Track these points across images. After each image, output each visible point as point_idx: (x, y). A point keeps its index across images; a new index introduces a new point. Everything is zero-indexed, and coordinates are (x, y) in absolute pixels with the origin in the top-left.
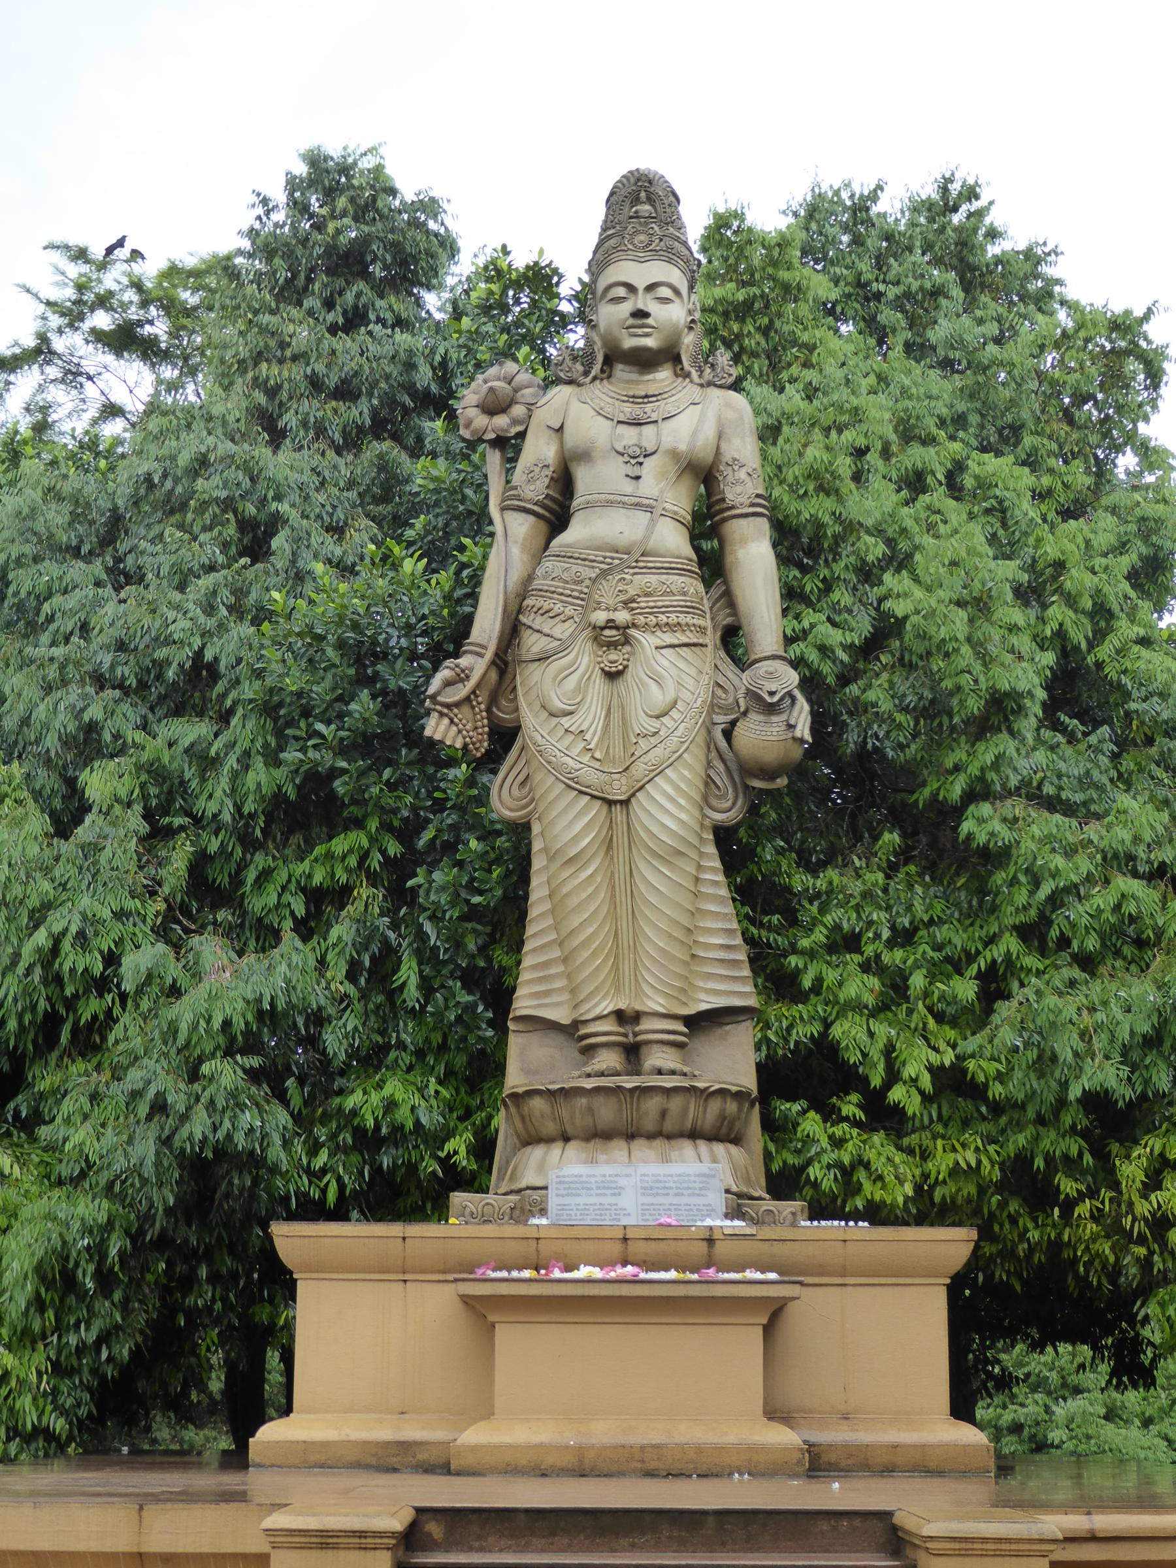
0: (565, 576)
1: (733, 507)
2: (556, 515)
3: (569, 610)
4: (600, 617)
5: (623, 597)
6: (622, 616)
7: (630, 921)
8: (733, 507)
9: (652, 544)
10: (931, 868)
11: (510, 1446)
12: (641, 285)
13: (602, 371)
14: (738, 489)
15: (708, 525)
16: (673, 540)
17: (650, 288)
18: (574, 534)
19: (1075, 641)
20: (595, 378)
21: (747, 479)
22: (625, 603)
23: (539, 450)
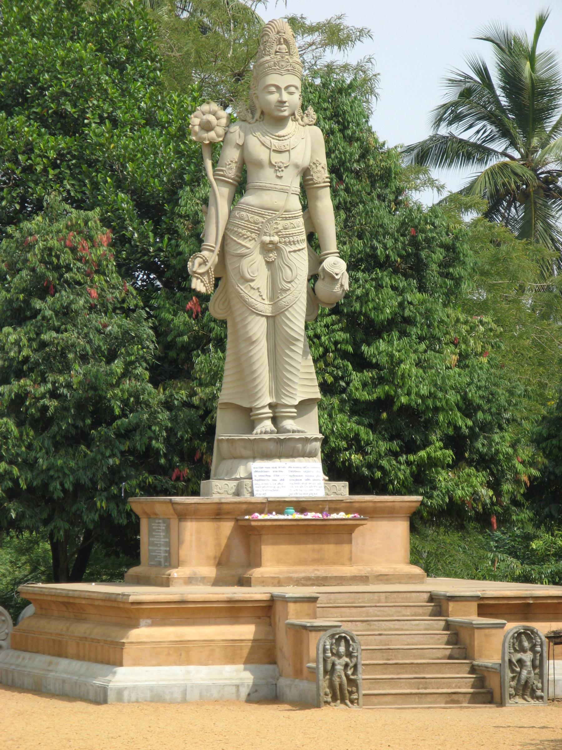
0: (251, 220)
1: (317, 183)
2: (241, 187)
3: (253, 235)
4: (267, 239)
5: (276, 230)
6: (276, 239)
7: (276, 371)
8: (317, 183)
9: (288, 207)
10: (344, 44)
11: (209, 624)
12: (283, 86)
13: (260, 118)
14: (319, 175)
15: (307, 191)
16: (295, 203)
17: (287, 88)
18: (249, 199)
19: (554, 114)
20: (257, 120)
21: (322, 170)
22: (277, 233)
23: (231, 155)
